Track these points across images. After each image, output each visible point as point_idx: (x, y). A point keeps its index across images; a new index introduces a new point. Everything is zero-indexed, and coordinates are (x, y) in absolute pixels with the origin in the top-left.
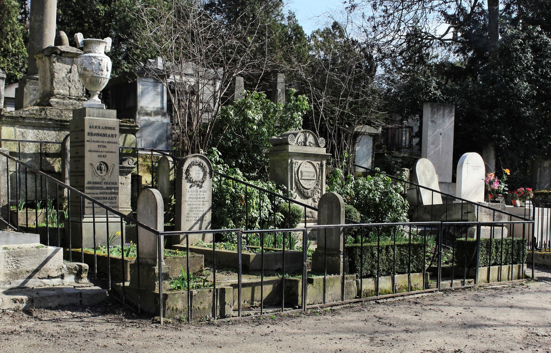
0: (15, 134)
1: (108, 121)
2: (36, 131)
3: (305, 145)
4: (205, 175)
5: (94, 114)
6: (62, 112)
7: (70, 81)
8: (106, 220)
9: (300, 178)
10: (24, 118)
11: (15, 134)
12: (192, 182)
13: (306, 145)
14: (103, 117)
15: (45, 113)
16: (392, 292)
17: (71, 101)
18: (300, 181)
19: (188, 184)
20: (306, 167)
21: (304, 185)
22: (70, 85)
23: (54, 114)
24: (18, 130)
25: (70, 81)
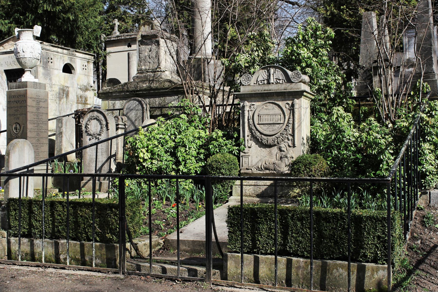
0: (109, 104)
1: (20, 91)
2: (121, 101)
3: (269, 83)
4: (102, 128)
5: (13, 87)
6: (138, 84)
7: (150, 58)
8: (46, 168)
9: (256, 123)
10: (111, 92)
11: (109, 104)
12: (90, 135)
13: (270, 83)
14: (19, 88)
15: (127, 87)
16: (53, 259)
17: (149, 73)
18: (258, 126)
19: (88, 136)
20: (266, 109)
21: (265, 132)
22: (150, 61)
23: (133, 86)
24: (110, 102)
25: (150, 58)
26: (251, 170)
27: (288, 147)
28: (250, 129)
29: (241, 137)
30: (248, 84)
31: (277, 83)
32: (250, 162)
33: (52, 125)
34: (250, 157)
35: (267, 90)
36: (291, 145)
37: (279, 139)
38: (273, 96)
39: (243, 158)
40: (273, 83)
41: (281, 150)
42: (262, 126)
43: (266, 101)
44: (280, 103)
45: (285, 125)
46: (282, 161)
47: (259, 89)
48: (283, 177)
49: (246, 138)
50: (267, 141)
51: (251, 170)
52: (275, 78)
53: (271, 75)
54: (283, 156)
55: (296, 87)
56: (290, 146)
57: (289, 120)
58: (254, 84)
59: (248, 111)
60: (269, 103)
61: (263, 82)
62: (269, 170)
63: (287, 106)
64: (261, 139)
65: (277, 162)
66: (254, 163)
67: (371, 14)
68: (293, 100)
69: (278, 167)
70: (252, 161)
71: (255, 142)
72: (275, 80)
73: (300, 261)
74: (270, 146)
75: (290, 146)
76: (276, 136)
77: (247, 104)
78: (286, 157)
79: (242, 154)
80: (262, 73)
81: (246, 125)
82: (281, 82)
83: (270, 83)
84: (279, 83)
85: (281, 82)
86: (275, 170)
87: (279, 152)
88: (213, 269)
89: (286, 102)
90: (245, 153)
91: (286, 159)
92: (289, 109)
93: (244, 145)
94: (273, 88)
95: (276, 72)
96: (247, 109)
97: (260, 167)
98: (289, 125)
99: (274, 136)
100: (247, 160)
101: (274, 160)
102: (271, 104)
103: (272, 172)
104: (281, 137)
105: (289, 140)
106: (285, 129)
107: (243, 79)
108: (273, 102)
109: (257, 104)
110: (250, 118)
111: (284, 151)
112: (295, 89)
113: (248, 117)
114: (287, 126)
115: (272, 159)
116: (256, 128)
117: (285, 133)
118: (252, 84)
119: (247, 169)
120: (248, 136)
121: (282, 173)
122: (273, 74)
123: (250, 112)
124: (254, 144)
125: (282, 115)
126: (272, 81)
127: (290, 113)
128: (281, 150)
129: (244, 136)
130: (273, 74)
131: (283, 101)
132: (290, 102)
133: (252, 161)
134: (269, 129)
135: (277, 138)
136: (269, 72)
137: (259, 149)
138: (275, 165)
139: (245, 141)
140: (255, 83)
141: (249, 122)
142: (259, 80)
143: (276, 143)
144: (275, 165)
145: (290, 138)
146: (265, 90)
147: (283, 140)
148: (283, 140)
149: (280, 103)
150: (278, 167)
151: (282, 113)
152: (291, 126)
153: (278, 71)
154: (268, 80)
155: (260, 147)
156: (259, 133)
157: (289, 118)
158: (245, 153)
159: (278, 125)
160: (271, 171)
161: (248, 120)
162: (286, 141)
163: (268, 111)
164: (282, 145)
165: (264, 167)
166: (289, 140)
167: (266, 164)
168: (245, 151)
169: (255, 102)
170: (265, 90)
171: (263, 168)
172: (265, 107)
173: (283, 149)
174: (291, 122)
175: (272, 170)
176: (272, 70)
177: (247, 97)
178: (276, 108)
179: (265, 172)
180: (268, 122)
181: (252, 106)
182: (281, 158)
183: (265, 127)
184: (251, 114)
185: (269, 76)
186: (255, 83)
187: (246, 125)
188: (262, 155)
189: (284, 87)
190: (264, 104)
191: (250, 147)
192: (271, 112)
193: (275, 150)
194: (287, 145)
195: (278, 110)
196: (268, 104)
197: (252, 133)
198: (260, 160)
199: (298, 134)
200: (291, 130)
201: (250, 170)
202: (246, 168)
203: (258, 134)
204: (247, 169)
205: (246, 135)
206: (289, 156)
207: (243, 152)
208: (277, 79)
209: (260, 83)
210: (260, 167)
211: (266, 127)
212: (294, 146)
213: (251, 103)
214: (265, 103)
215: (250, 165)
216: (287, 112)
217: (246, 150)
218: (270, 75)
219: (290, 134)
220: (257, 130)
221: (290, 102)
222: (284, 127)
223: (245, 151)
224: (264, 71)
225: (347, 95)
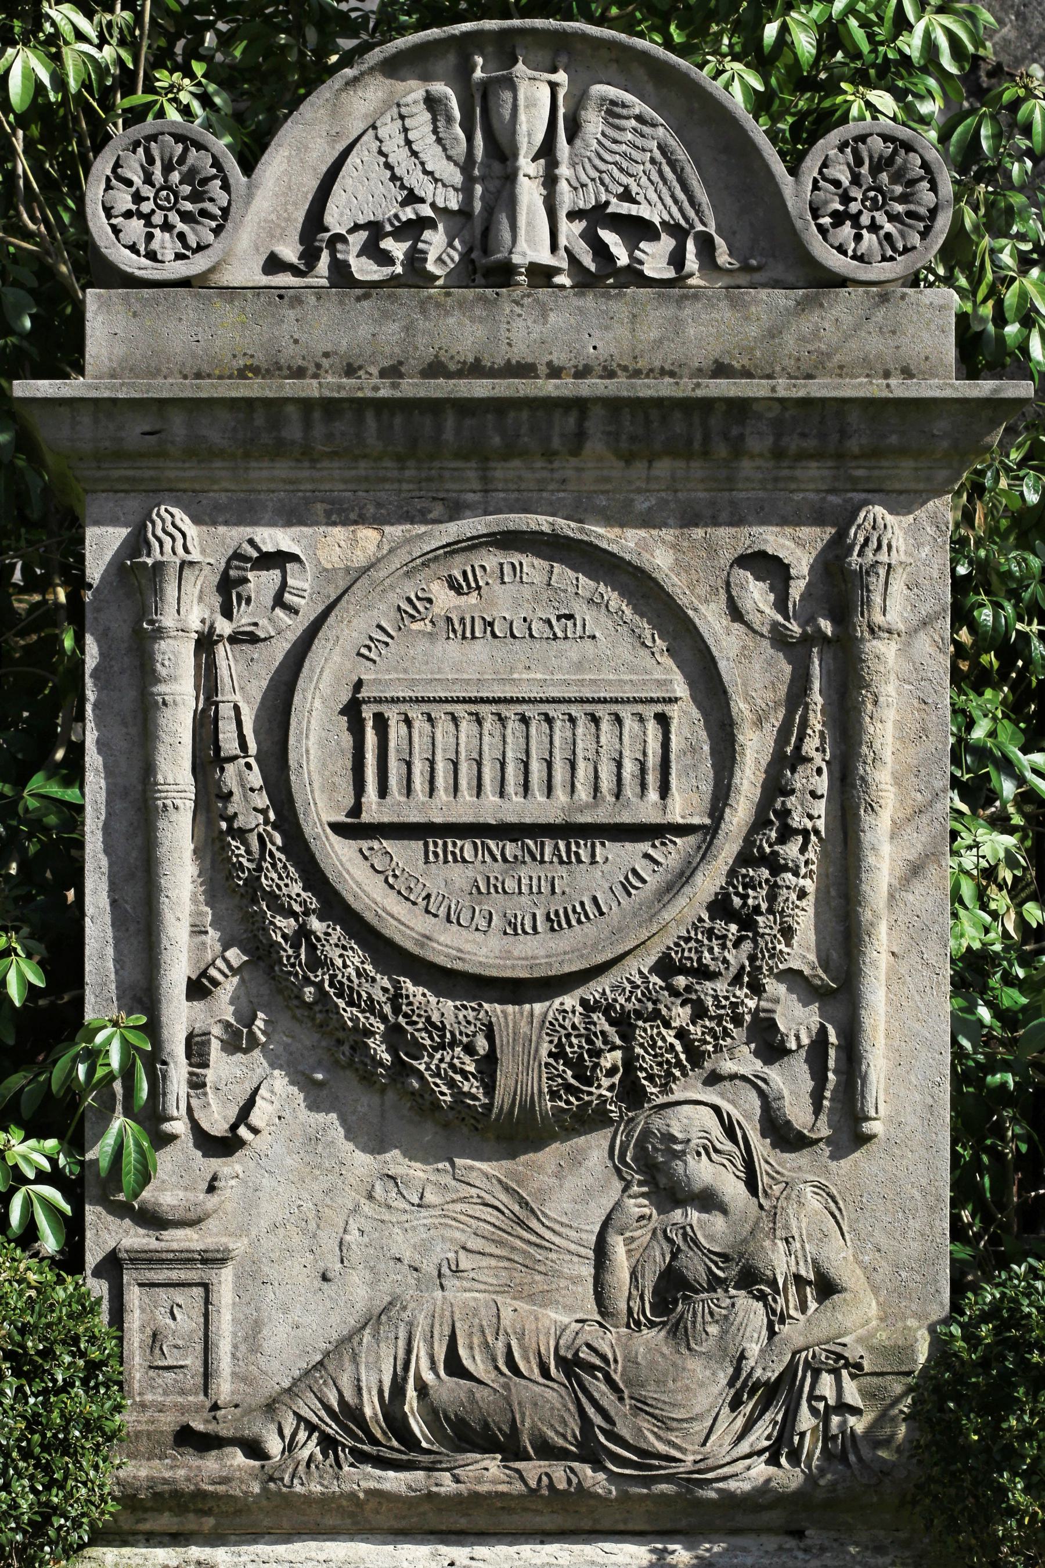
3: (487, 268)
9: (320, 804)
18: (341, 858)
20: (456, 628)
21: (481, 951)
26: (254, 1449)
27: (760, 1146)
28: (236, 896)
29: (100, 1000)
30: (197, 265)
31: (601, 276)
32: (224, 1348)
33: (796, 1439)
34: (225, 1280)
35: (476, 369)
36: (798, 1113)
37: (644, 1031)
38: (578, 440)
39: (133, 1296)
40: (542, 275)
41: (669, 1191)
42: (405, 854)
43: (455, 511)
44: (657, 551)
45: (728, 849)
46: (679, 1333)
47: (340, 342)
49: (179, 1016)
50: (488, 1065)
51: (254, 1449)
52: (567, 198)
53: (528, 167)
54: (695, 1267)
55: (874, 344)
56: (783, 1135)
57: (775, 786)
58: (274, 264)
59: (206, 643)
60: (508, 541)
61: (397, 249)
62: (510, 1449)
63: (757, 595)
64: (394, 1035)
65: (608, 1341)
66: (281, 1360)
68: (844, 520)
69: (641, 1406)
70: (252, 1336)
71: (302, 1080)
72: (570, 231)
74: (517, 1133)
75: (783, 1135)
76: (593, 990)
77: (190, 542)
78: (751, 1278)
79: (106, 1233)
80: (389, 129)
81: (178, 837)
82: (655, 256)
83: (502, 274)
84: (634, 276)
85: (655, 256)
86: (590, 1453)
87: (637, 1206)
89: (733, 541)
90: (152, 1219)
91: (751, 1314)
92: (779, 638)
93: (152, 1118)
94: (557, 337)
95: (594, 123)
96: (187, 609)
97: (371, 1408)
98: (791, 850)
99: (570, 1001)
100: (187, 1322)
101: (564, 1315)
102: (533, 567)
103: (558, 1472)
104: (681, 1015)
105: (770, 1045)
106: (720, 907)
107: (123, 200)
108: (567, 527)
109: (329, 548)
110: (229, 743)
111: (708, 1200)
112: (869, 367)
113: (206, 726)
114: (746, 858)
115: (542, 1298)
116: (315, 877)
117: (738, 957)
118: (245, 271)
119: (191, 1440)
120: (199, 989)
121: (691, 1482)
122: (547, 151)
123: (221, 651)
124: (279, 1096)
125: (687, 721)
126: (531, 246)
127: (797, 696)
128: (669, 1191)
129: (143, 995)
130: (547, 151)
131: (689, 519)
132: (798, 549)
133: (252, 1336)
134: (496, 903)
135: (624, 1023)
136: (485, 109)
137: (362, 1162)
138: (599, 1388)
139: (156, 1060)
140: (290, 253)
141: (211, 798)
142: (336, 219)
143: (604, 1087)
144: (599, 1388)
145: (797, 1019)
146: (435, 369)
147: (696, 1057)
148: (696, 1057)
149: (657, 551)
150: (641, 1406)
151: (681, 689)
152: (805, 864)
153: (612, 110)
154: (480, 230)
155: (376, 1144)
156: (356, 957)
157: (786, 760)
158: (152, 1219)
159: (624, 855)
160: (533, 1469)
161: (208, 759)
162: (743, 1061)
163: (480, 650)
164: (691, 1116)
165: (433, 1414)
166: (770, 1045)
167: (455, 1366)
168: (166, 1193)
169: (292, 516)
170: (435, 369)
171: (417, 1426)
172: (444, 599)
173: (702, 1171)
174: (811, 811)
175: (547, 1451)
176: (534, 100)
177: (197, 452)
179: (446, 1484)
181: (261, 583)
182: (672, 1291)
183: (452, 877)
184: (244, 685)
185: (494, 166)
186: (290, 253)
187: (178, 837)
188: (401, 1244)
189: (704, 333)
190: (430, 559)
191: (224, 1146)
192: (540, 671)
193: (579, 1183)
194: (745, 1110)
195: (625, 649)
196: (491, 559)
197: (261, 954)
198: (376, 1319)
199: (895, 978)
200: (805, 921)
201: (238, 1458)
202: (169, 1422)
203: (351, 961)
204: (191, 1440)
205: (177, 970)
206: (780, 1262)
207: (122, 1210)
208: (596, 216)
209: (364, 269)
210: (371, 1408)
211: (459, 876)
212: (851, 1132)
213: (234, 536)
214: (453, 549)
215: (225, 1388)
216: (754, 678)
217: (174, 1178)
218: (502, 153)
219: (792, 977)
220: (334, 905)
221: (798, 549)
222: (709, 882)
223: (166, 1193)
224: (414, 91)
225: (172, 55)
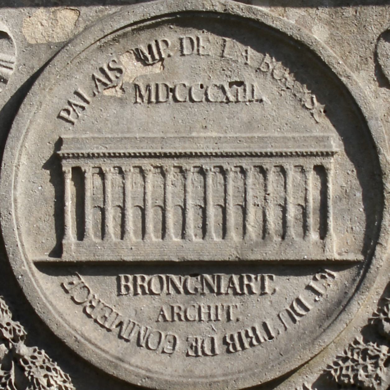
18: (48, 294)
42: (101, 288)
48: (159, 20)
67: (64, 279)
73: (182, 149)
88: (140, 276)
102: (209, 42)
125: (342, 174)
134: (179, 330)
151: (335, 143)
163: (164, 113)
172: (132, 68)
178: (270, 87)
180: (174, 248)
190: (119, 36)
192: (212, 131)
195: (288, 111)
196: (171, 36)
211: (146, 304)
214: (139, 27)
